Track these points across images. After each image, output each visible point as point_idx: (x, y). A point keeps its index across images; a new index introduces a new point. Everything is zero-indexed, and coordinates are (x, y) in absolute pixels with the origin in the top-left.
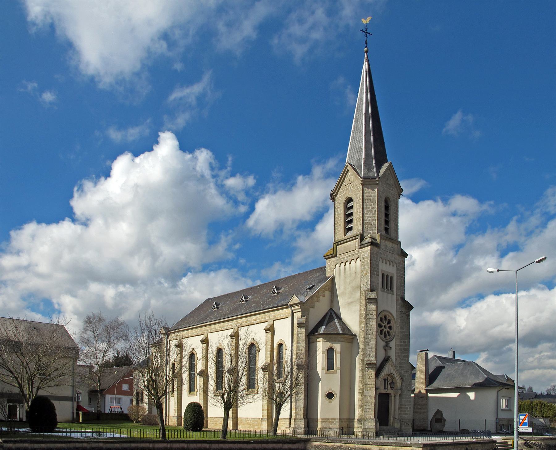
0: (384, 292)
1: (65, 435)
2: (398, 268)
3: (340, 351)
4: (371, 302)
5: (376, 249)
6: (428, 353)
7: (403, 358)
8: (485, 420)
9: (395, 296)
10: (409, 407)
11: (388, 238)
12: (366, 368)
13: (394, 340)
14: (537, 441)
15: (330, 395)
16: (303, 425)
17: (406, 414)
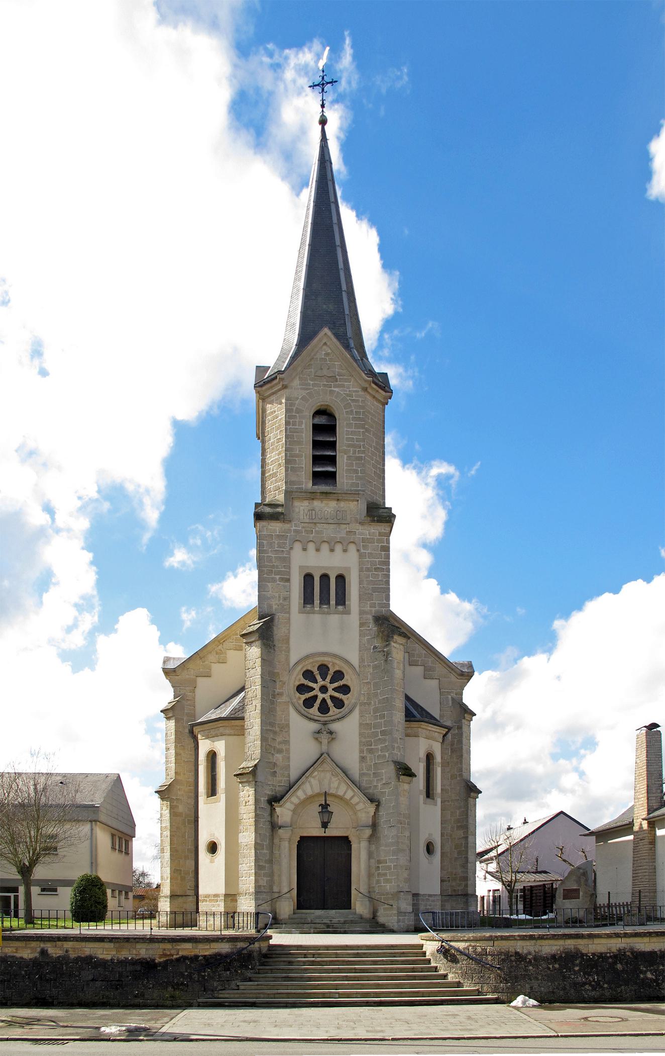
0: (314, 613)
1: (7, 925)
2: (362, 551)
3: (224, 755)
4: (252, 642)
5: (275, 527)
6: (659, 731)
7: (380, 754)
8: (609, 892)
9: (354, 618)
10: (394, 865)
11: (319, 494)
12: (240, 785)
13: (356, 712)
14: (473, 944)
15: (213, 848)
16: (169, 908)
17: (387, 881)
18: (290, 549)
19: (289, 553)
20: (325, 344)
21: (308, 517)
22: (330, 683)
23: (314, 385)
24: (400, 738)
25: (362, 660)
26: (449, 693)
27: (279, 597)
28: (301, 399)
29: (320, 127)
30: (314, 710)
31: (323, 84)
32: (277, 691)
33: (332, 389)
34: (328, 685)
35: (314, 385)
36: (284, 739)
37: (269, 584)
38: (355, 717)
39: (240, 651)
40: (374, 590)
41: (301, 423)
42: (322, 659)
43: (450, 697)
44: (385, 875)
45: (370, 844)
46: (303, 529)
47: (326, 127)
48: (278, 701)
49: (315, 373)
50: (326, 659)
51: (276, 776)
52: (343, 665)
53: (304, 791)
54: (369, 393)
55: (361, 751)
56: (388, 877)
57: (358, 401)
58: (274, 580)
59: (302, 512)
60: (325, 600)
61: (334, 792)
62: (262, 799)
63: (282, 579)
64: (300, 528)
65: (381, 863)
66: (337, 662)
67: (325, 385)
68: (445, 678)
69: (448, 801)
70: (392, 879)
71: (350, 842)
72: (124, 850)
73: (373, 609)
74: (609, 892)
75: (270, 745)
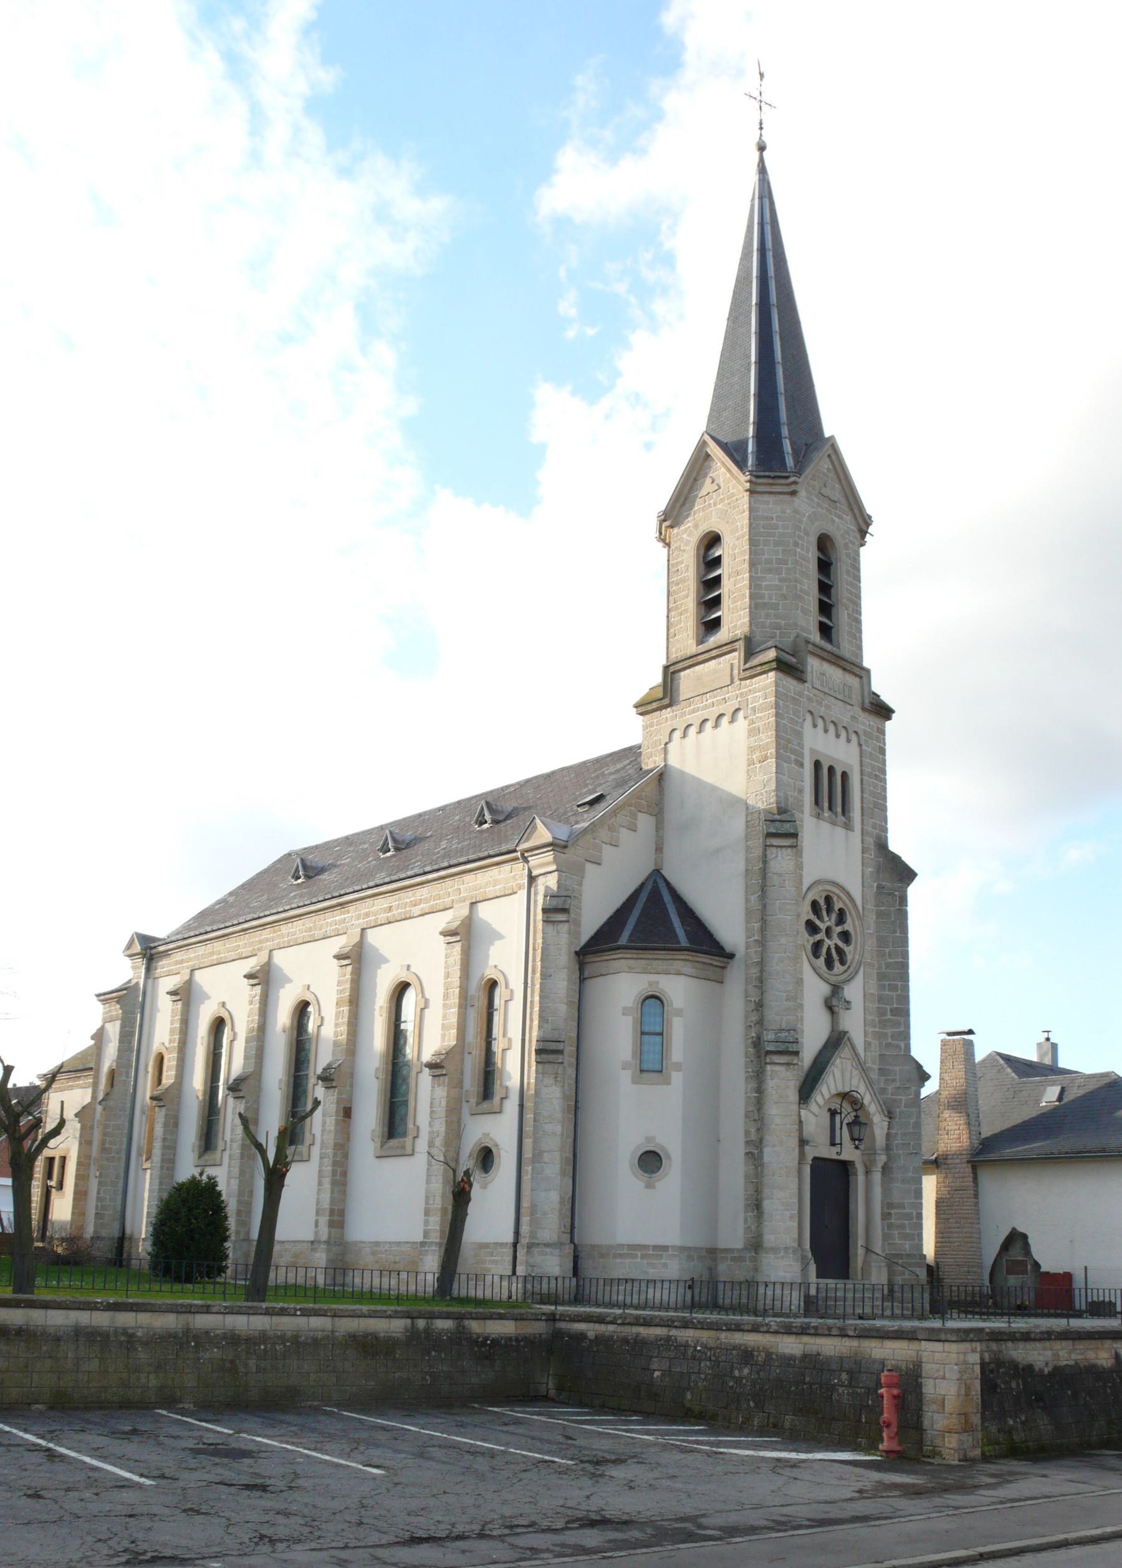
8: (62, 1102)
29: (757, 154)
31: (761, 101)
39: (595, 865)
44: (903, 1227)
47: (765, 153)
56: (908, 1231)
65: (893, 1208)
70: (913, 1235)
71: (84, 1108)
72: (569, 1526)
74: (62, 1102)
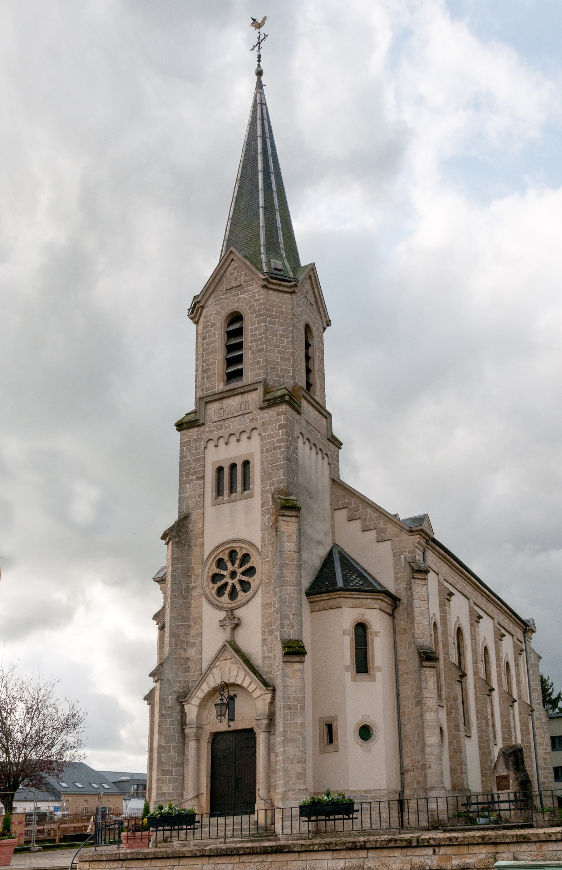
5: (193, 432)
9: (257, 500)
18: (204, 449)
19: (204, 453)
20: (233, 260)
21: (218, 415)
22: (239, 568)
23: (226, 298)
24: (293, 614)
25: (263, 540)
26: (401, 553)
27: (195, 496)
28: (216, 314)
30: (225, 598)
32: (192, 585)
33: (240, 296)
34: (237, 570)
35: (226, 298)
36: (197, 632)
37: (187, 485)
38: (258, 601)
40: (273, 468)
41: (215, 334)
42: (230, 545)
43: (402, 556)
45: (270, 735)
46: (215, 428)
47: (262, 78)
48: (193, 594)
49: (226, 287)
50: (234, 545)
51: (189, 672)
52: (248, 548)
53: (208, 684)
54: (205, 303)
55: (263, 633)
57: (260, 299)
58: (191, 481)
59: (213, 413)
60: (232, 489)
61: (233, 681)
62: (170, 697)
63: (198, 479)
64: (213, 428)
66: (243, 545)
67: (234, 296)
68: (397, 537)
69: (407, 674)
73: (273, 487)
75: (181, 641)
